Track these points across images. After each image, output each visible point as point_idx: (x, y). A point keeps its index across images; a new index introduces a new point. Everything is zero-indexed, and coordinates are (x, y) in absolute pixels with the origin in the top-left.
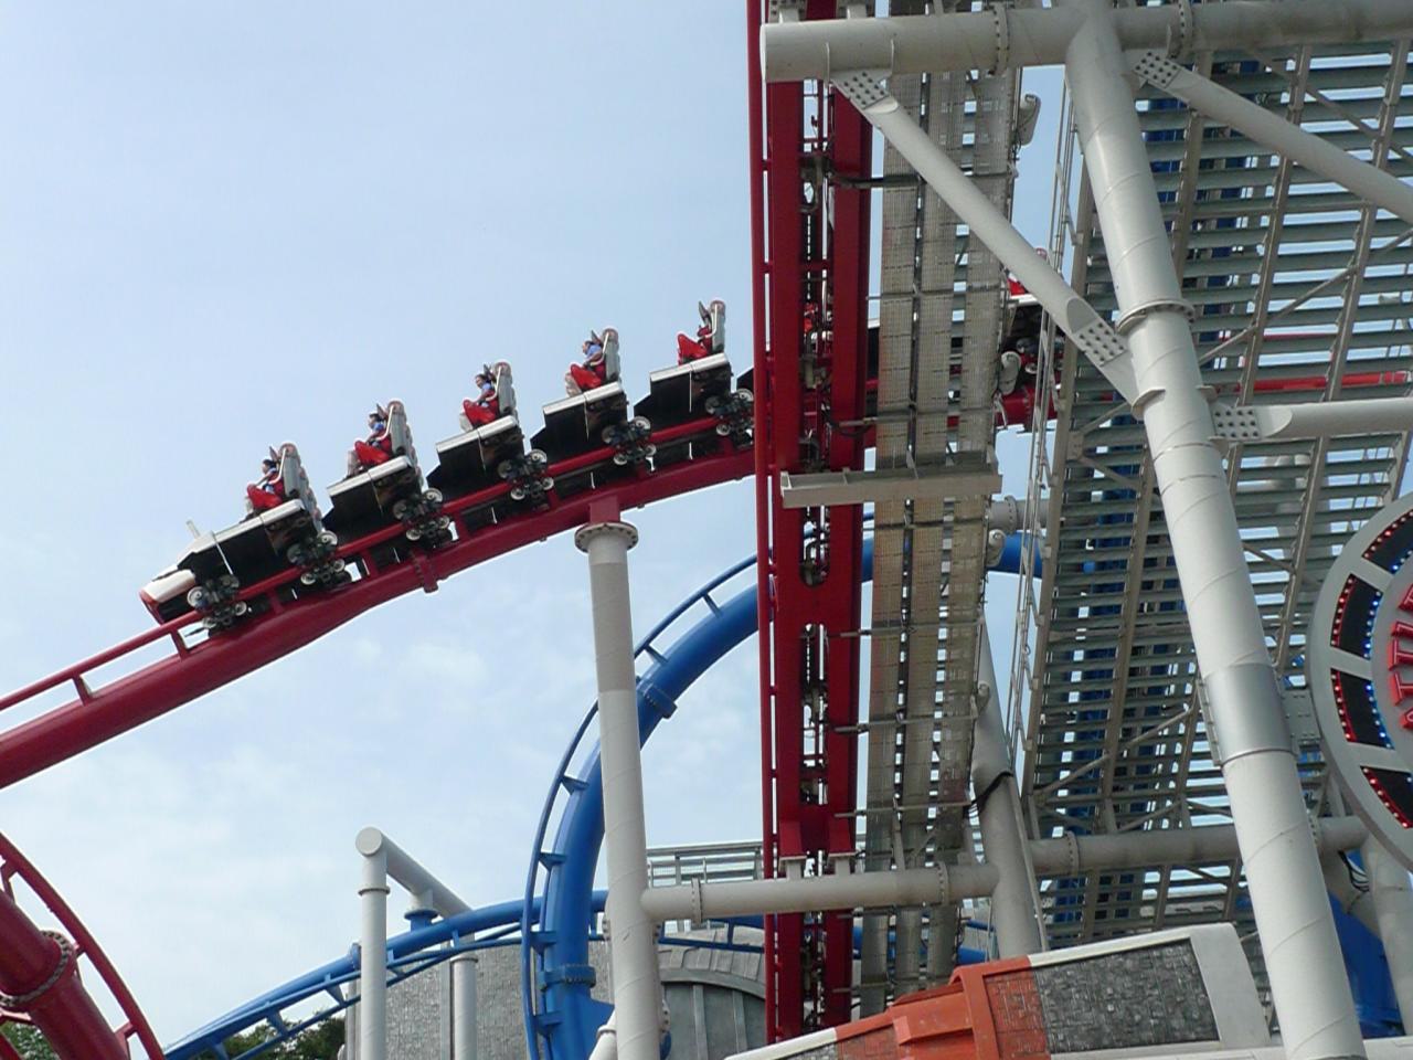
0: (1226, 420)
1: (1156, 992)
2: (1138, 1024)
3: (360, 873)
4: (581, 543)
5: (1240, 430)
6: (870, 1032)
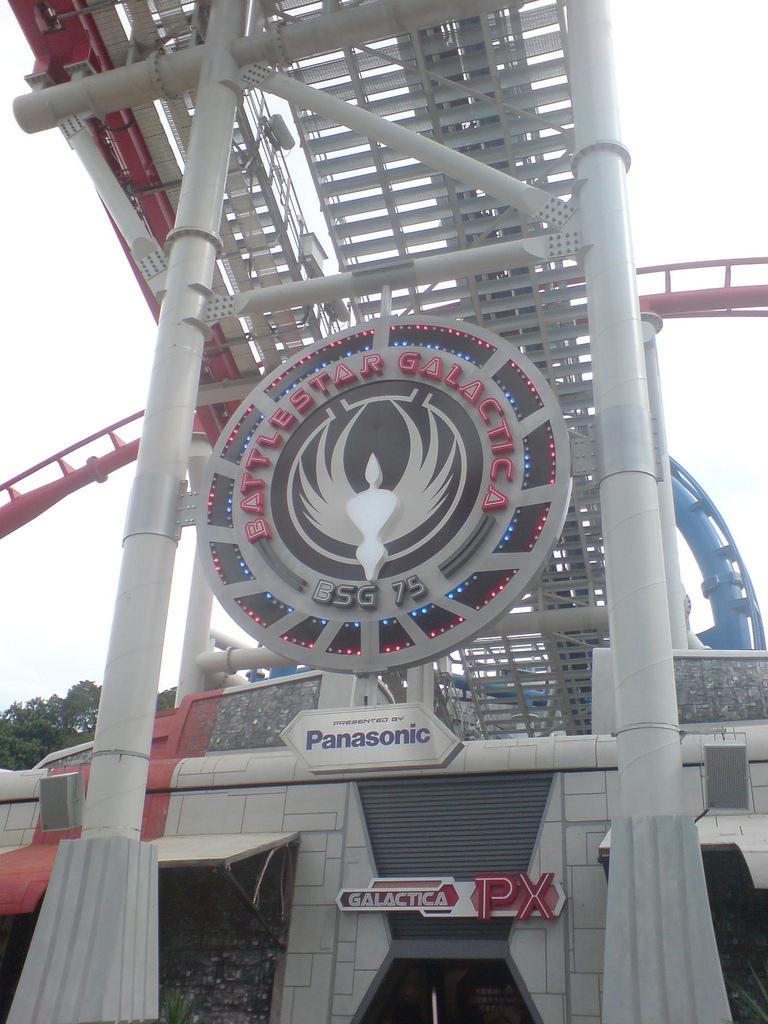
1: (287, 712)
5: (218, 313)
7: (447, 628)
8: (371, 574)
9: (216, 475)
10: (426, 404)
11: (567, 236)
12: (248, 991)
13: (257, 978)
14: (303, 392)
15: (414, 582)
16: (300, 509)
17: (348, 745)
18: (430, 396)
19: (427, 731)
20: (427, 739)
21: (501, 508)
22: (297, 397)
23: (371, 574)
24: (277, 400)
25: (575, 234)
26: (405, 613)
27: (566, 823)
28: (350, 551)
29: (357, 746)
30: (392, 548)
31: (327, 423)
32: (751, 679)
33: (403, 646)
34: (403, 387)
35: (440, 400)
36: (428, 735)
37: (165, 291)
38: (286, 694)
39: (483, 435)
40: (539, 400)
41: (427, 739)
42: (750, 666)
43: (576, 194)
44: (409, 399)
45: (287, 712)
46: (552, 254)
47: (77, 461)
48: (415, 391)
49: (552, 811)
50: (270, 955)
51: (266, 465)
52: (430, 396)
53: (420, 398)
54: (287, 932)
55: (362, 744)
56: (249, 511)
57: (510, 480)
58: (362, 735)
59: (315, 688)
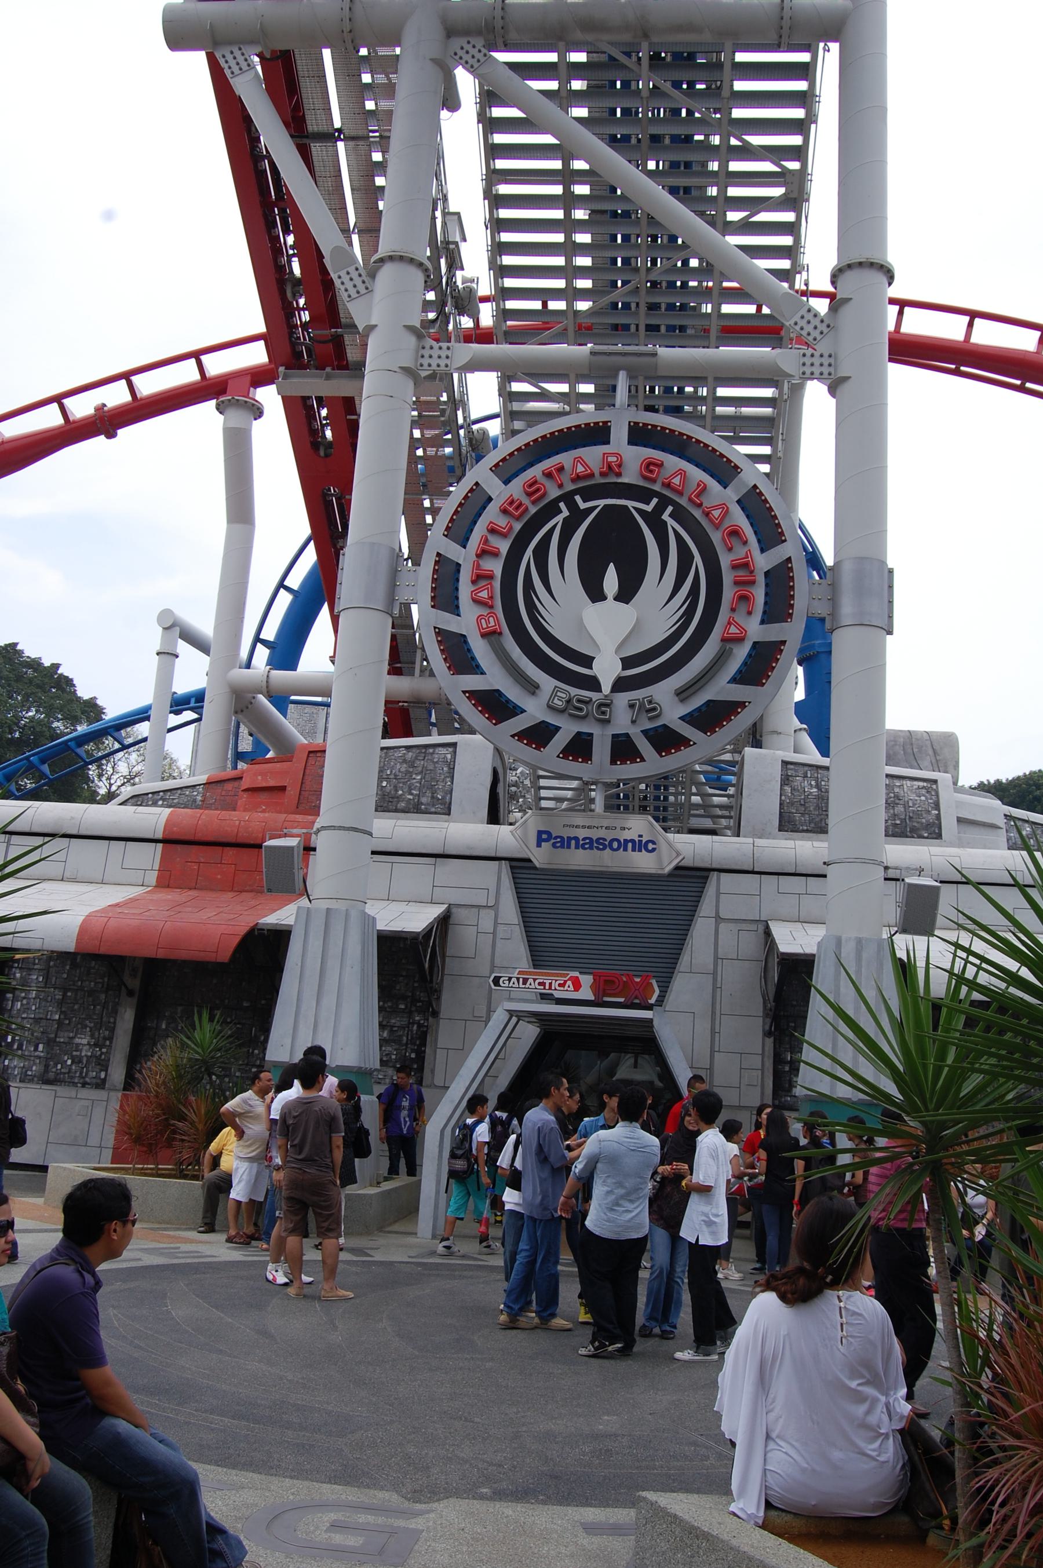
0: (426, 352)
1: (419, 777)
2: (398, 798)
3: (155, 638)
4: (220, 409)
5: (434, 362)
6: (229, 780)
7: (678, 750)
8: (606, 687)
9: (438, 555)
10: (665, 517)
11: (822, 356)
12: (395, 1049)
13: (405, 1038)
14: (535, 482)
15: (650, 702)
16: (531, 607)
17: (577, 847)
18: (670, 509)
19: (654, 843)
20: (654, 850)
21: (740, 640)
22: (531, 486)
23: (606, 687)
24: (506, 482)
25: (830, 356)
26: (639, 731)
27: (718, 919)
28: (587, 661)
29: (586, 849)
30: (628, 662)
31: (559, 519)
32: (897, 797)
33: (633, 761)
34: (642, 494)
35: (680, 515)
36: (654, 846)
37: (373, 327)
38: (416, 758)
39: (725, 560)
40: (782, 534)
41: (654, 850)
42: (898, 784)
43: (834, 308)
44: (649, 508)
45: (419, 777)
46: (804, 373)
47: (81, 407)
48: (655, 501)
49: (706, 907)
50: (417, 1018)
51: (495, 554)
52: (670, 509)
53: (659, 509)
54: (439, 998)
55: (591, 848)
56: (477, 601)
57: (750, 613)
58: (591, 839)
59: (449, 756)
